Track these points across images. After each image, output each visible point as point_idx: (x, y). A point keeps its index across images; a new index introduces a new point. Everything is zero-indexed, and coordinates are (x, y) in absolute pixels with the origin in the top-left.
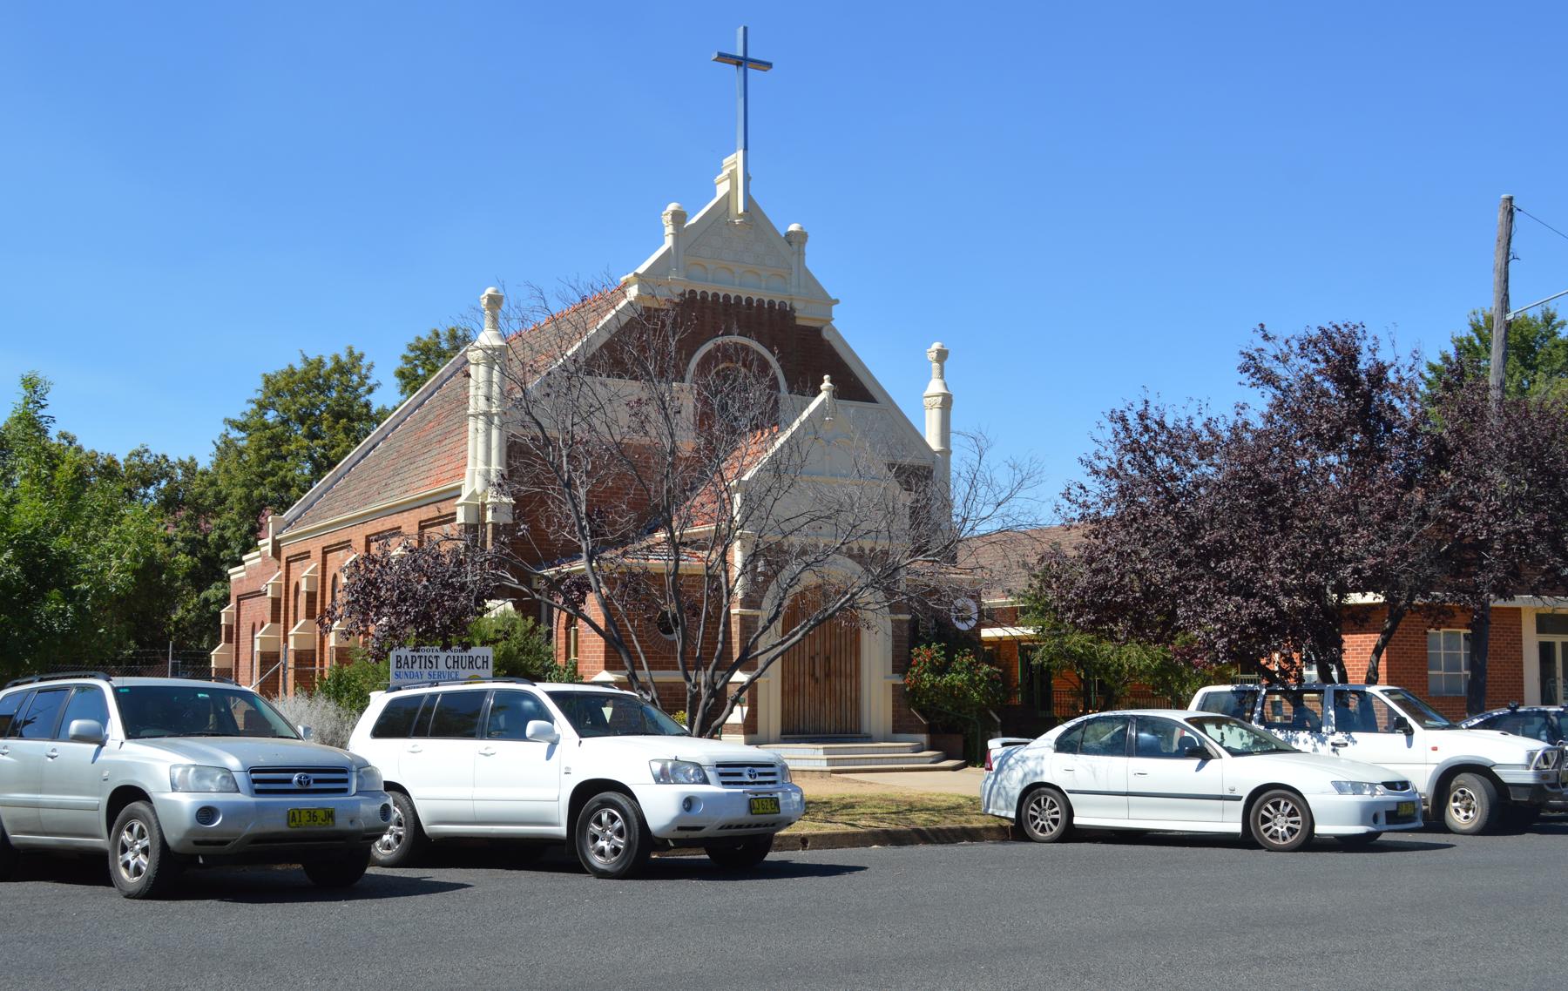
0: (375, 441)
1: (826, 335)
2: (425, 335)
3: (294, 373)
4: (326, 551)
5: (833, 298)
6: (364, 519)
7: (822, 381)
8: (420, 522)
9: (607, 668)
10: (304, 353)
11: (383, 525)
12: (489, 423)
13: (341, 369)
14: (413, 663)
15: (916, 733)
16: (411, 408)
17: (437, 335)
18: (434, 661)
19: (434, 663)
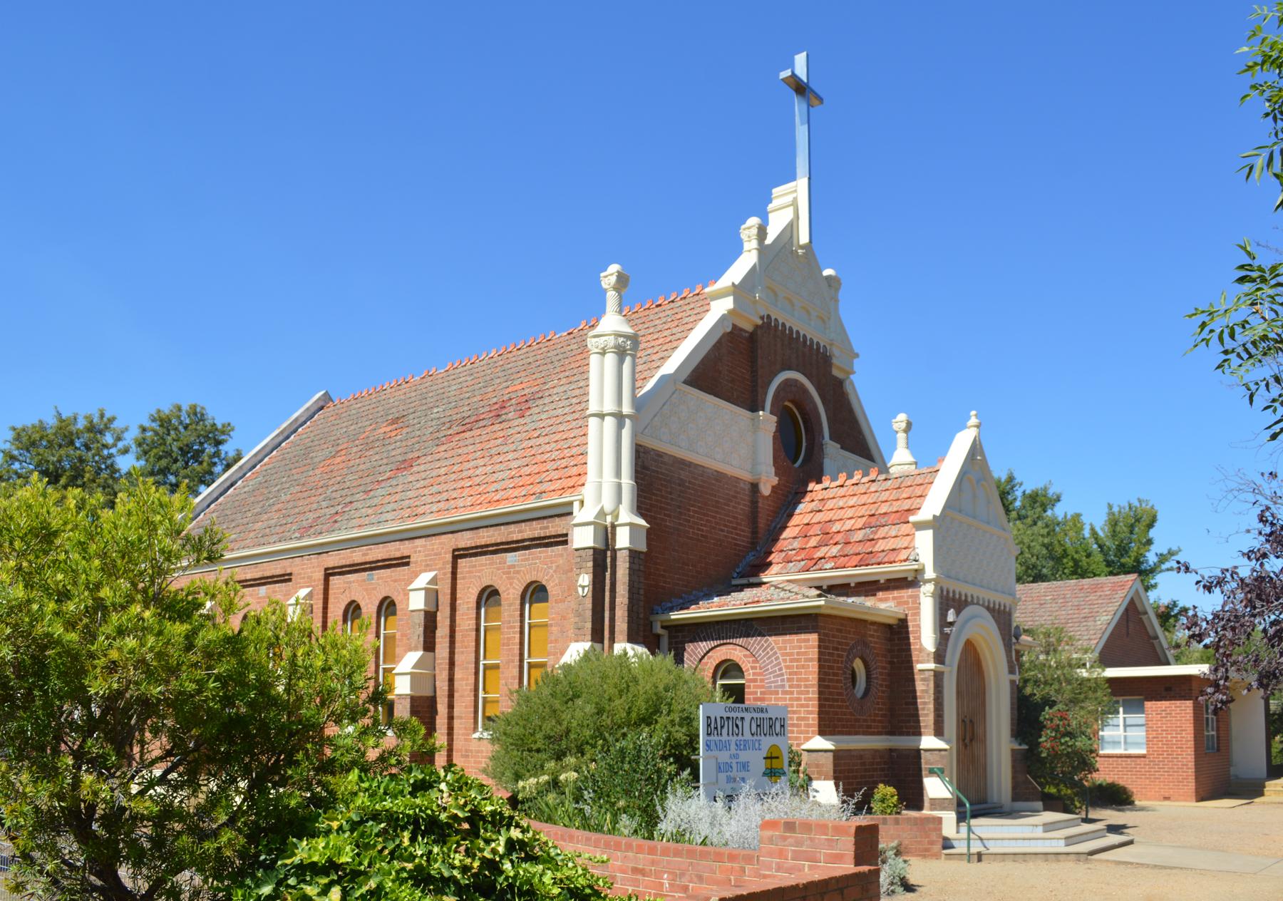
0: (234, 479)
1: (848, 388)
2: (166, 409)
3: (35, 427)
4: (329, 574)
5: (856, 351)
6: (322, 550)
7: (969, 418)
8: (454, 550)
9: (822, 733)
10: (59, 409)
11: (363, 555)
12: (620, 426)
13: (91, 428)
14: (722, 727)
15: (1033, 800)
16: (268, 449)
17: (180, 409)
18: (739, 723)
19: (740, 726)
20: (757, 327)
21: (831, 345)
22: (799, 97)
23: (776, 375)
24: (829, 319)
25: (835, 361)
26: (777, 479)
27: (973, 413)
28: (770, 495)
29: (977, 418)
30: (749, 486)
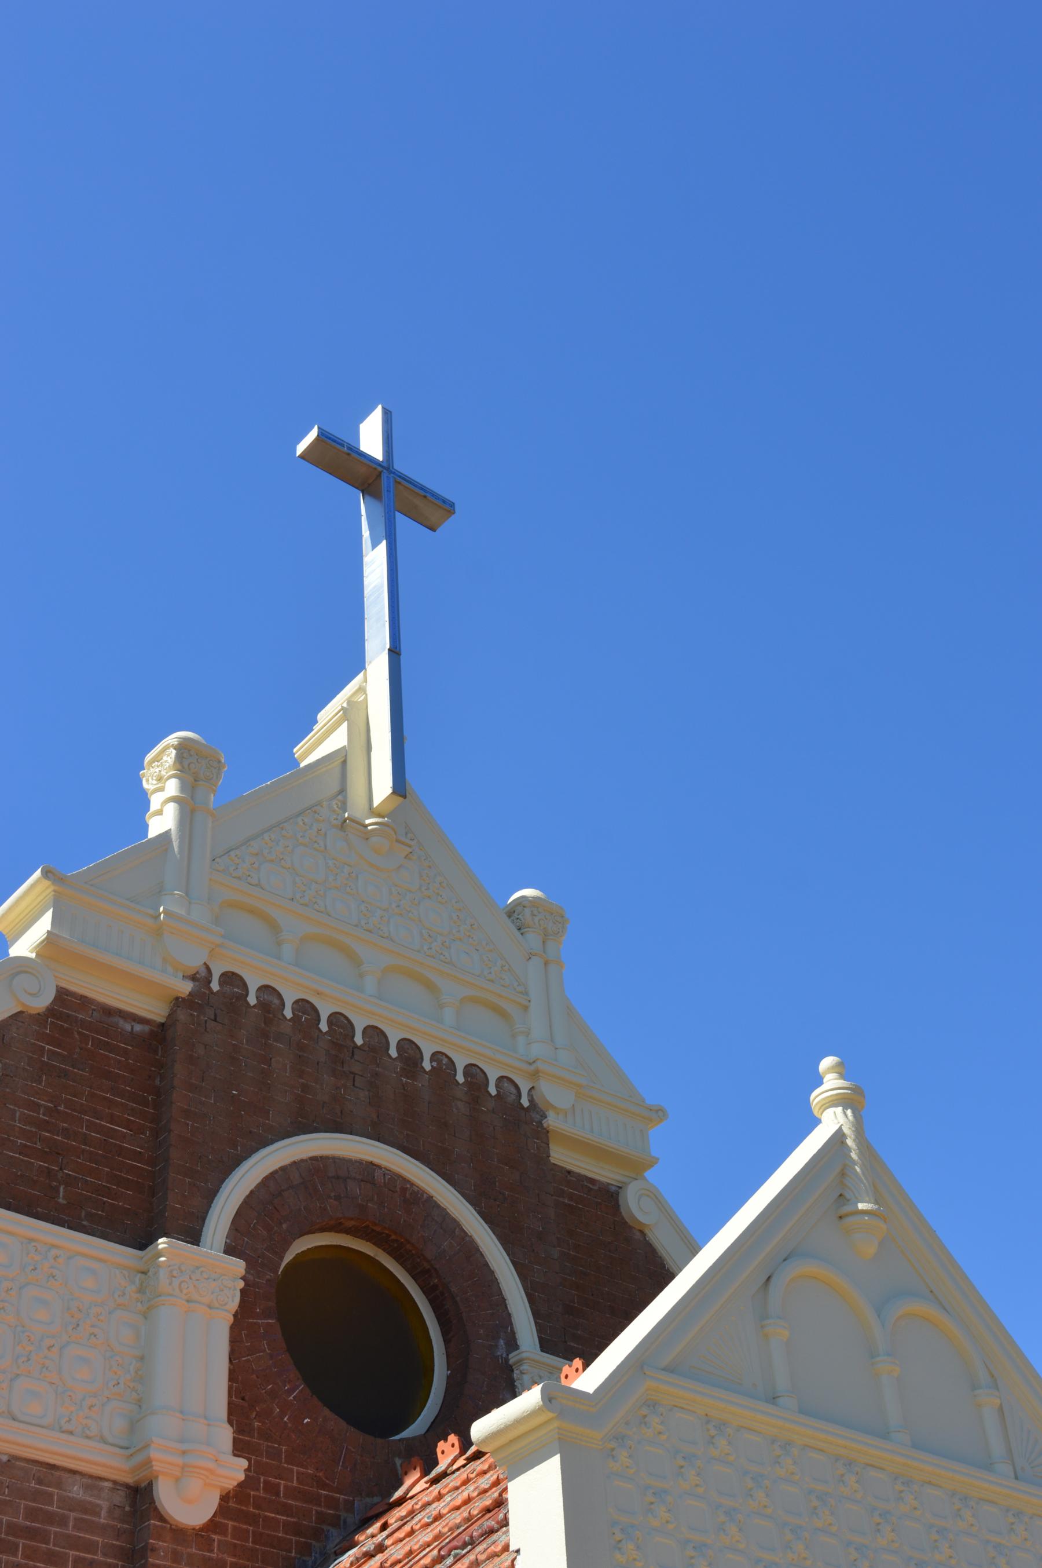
7: (819, 1081)
20: (178, 1002)
21: (535, 1075)
22: (367, 497)
23: (265, 1143)
24: (526, 1008)
25: (552, 1121)
26: (244, 1463)
27: (827, 1062)
28: (212, 1526)
29: (842, 1076)
30: (120, 1498)
